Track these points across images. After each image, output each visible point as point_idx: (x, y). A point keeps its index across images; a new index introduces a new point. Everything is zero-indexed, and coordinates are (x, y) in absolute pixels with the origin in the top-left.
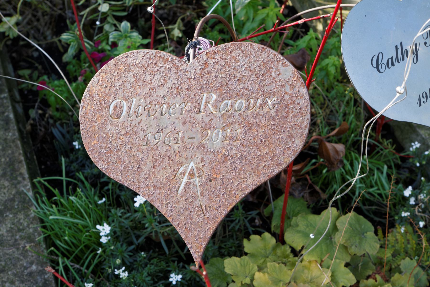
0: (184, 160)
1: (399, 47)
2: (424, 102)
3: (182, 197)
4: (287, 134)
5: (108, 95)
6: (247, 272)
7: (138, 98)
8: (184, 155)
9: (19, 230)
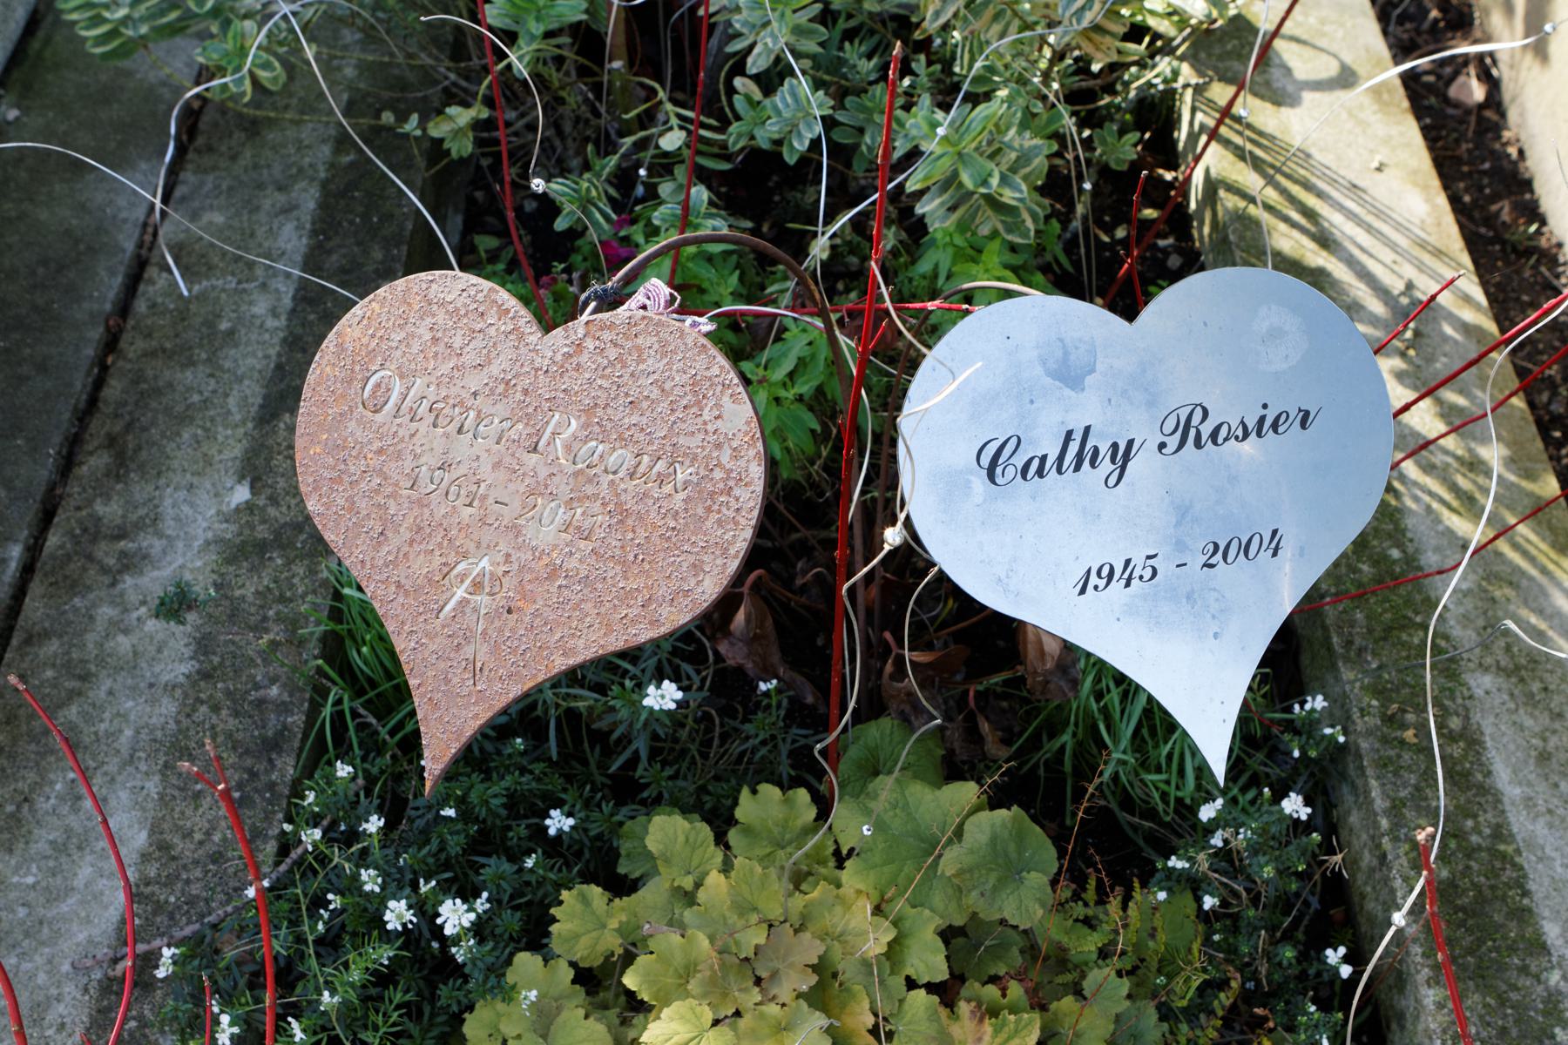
0: (472, 546)
1: (1077, 436)
2: (1096, 588)
3: (443, 627)
4: (692, 559)
5: (372, 354)
6: (695, 863)
7: (426, 379)
8: (475, 537)
9: (282, 599)
